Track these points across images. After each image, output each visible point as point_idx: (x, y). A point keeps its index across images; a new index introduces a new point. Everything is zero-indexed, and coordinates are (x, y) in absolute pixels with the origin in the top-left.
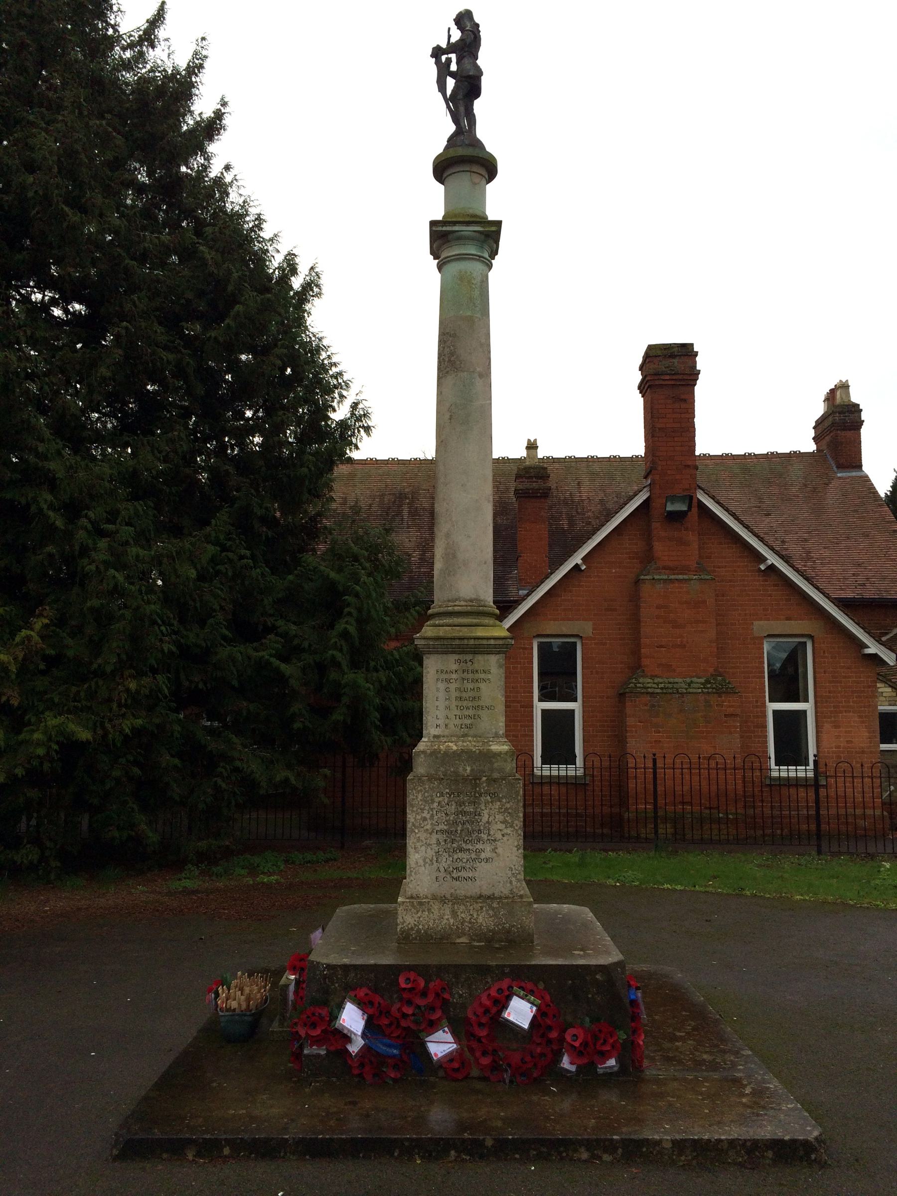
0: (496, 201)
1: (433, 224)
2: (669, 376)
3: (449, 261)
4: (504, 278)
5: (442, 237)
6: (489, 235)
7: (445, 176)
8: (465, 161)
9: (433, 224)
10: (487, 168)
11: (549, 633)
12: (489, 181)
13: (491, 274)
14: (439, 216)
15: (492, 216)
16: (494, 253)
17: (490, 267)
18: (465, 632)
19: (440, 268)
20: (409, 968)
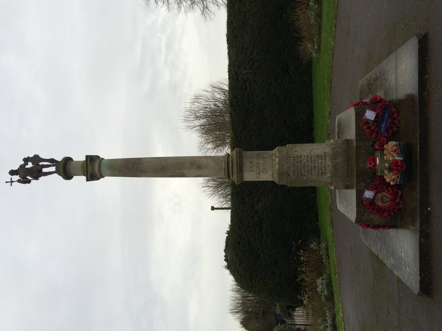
0: (79, 157)
1: (87, 180)
2: (11, 185)
3: (101, 174)
4: (108, 153)
5: (92, 176)
6: (91, 159)
7: (70, 176)
8: (66, 168)
9: (87, 180)
10: (68, 160)
11: (221, 210)
12: (72, 160)
13: (105, 158)
14: (84, 178)
15: (84, 159)
16: (98, 157)
17: (103, 159)
18: (235, 162)
19: (103, 177)
20: (357, 186)
